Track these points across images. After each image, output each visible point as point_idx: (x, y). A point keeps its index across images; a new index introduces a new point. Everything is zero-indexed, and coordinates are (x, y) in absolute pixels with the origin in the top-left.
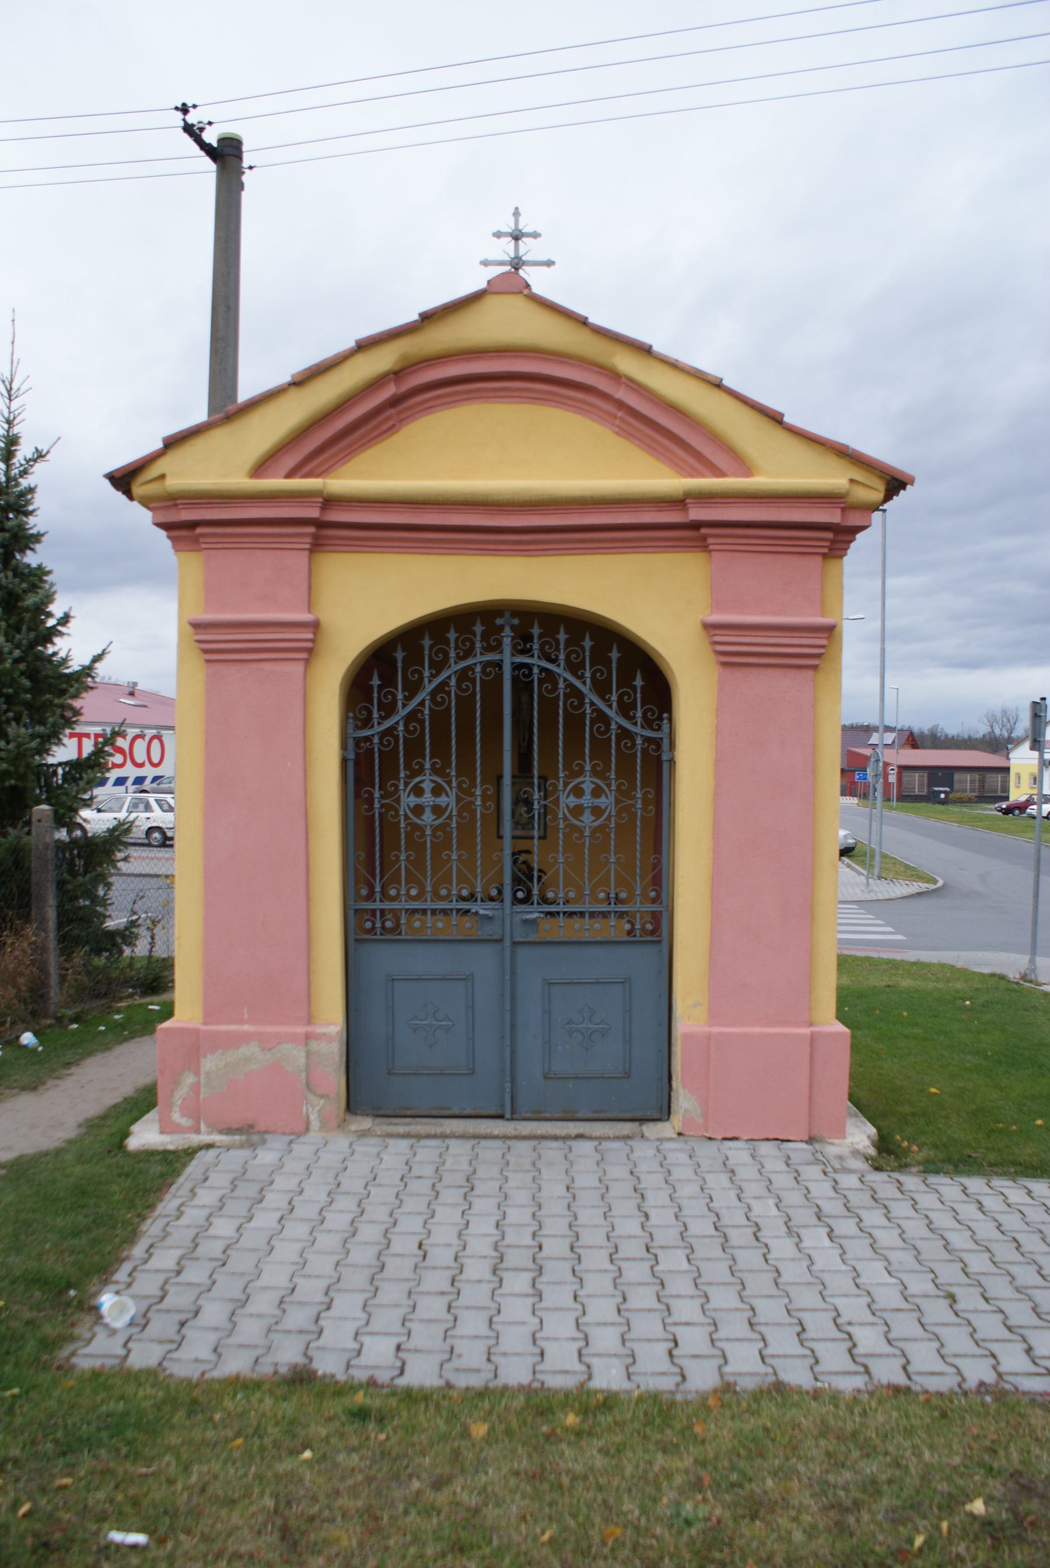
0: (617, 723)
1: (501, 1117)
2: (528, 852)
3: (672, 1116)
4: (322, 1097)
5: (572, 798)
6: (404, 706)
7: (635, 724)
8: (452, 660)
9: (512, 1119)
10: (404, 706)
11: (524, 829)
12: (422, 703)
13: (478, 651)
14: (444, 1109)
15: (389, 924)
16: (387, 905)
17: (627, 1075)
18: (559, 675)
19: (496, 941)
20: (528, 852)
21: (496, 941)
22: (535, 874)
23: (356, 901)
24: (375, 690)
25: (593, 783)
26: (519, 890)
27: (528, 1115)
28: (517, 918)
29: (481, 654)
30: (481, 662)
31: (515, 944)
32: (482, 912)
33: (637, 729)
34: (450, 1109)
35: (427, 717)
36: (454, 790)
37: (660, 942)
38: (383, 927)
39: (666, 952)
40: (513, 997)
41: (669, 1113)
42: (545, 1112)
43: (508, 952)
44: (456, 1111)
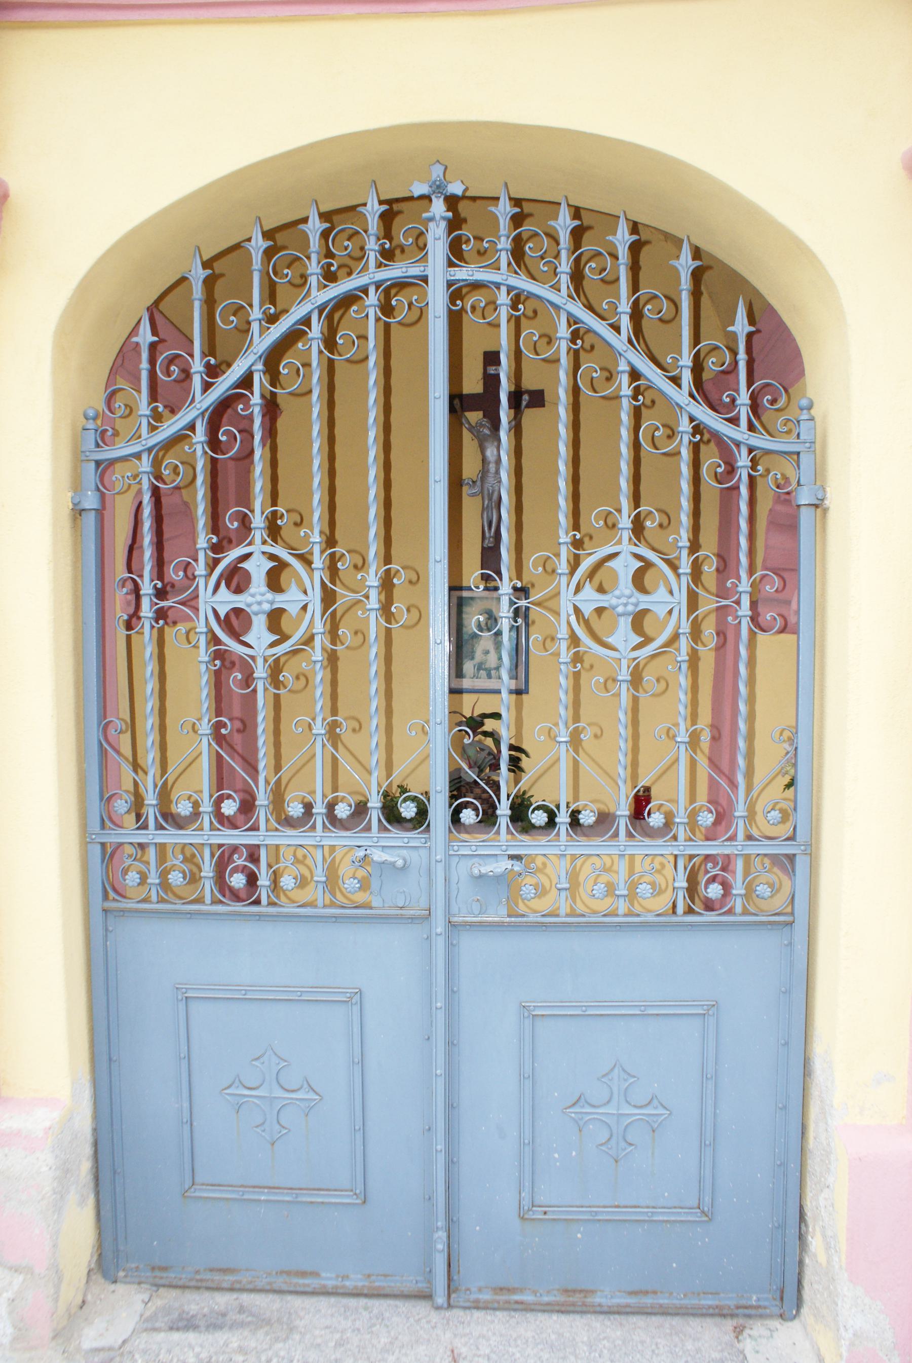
0: (692, 419)
1: (426, 1296)
2: (497, 716)
3: (805, 1310)
4: (16, 1270)
5: (588, 591)
6: (207, 387)
7: (734, 421)
8: (313, 281)
9: (450, 1306)
10: (207, 387)
11: (489, 676)
12: (246, 381)
13: (372, 263)
14: (303, 1274)
15: (176, 878)
16: (171, 837)
17: (708, 1216)
18: (557, 308)
19: (413, 919)
20: (497, 716)
21: (413, 919)
22: (505, 753)
23: (103, 826)
24: (145, 355)
25: (638, 557)
26: (466, 805)
27: (486, 1296)
28: (462, 870)
29: (379, 265)
30: (378, 285)
31: (451, 925)
32: (378, 856)
33: (739, 433)
34: (315, 1274)
35: (257, 410)
36: (317, 575)
37: (791, 924)
38: (165, 885)
39: (800, 948)
40: (451, 1044)
41: (799, 1303)
42: (521, 1290)
43: (440, 944)
44: (329, 1279)
